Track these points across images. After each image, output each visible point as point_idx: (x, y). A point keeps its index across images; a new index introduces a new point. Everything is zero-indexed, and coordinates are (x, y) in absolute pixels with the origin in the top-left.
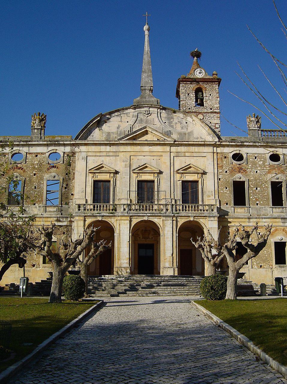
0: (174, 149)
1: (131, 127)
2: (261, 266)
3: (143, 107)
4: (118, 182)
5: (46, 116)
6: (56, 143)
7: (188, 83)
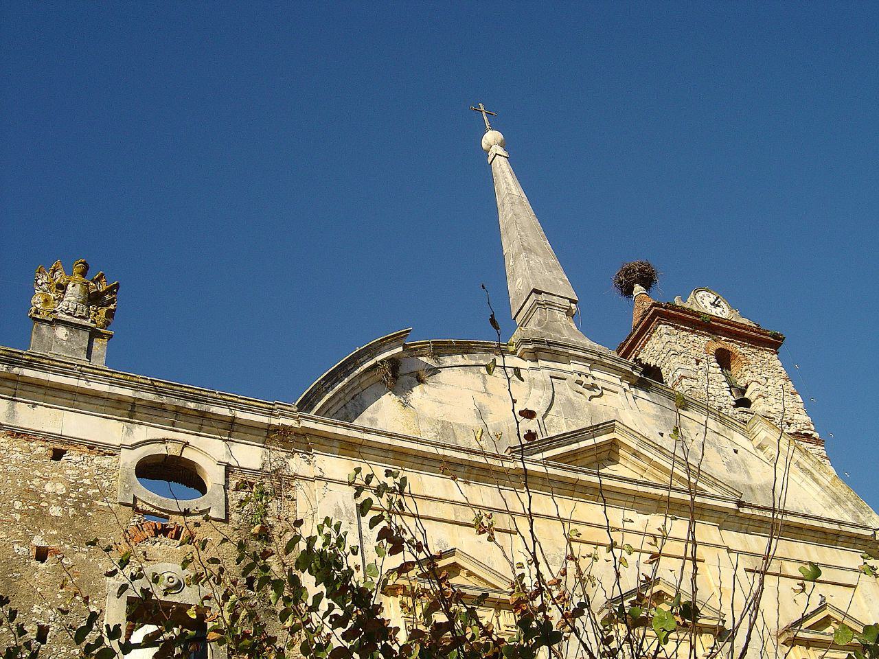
3: (569, 358)
5: (117, 286)
6: (192, 405)
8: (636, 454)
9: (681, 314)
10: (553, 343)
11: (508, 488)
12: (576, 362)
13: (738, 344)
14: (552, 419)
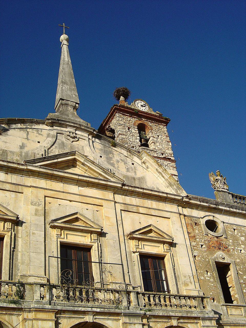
1: (45, 150)
3: (66, 126)
4: (20, 242)
8: (83, 164)
9: (126, 109)
10: (60, 120)
11: (24, 176)
12: (70, 127)
13: (150, 122)
14: (53, 150)
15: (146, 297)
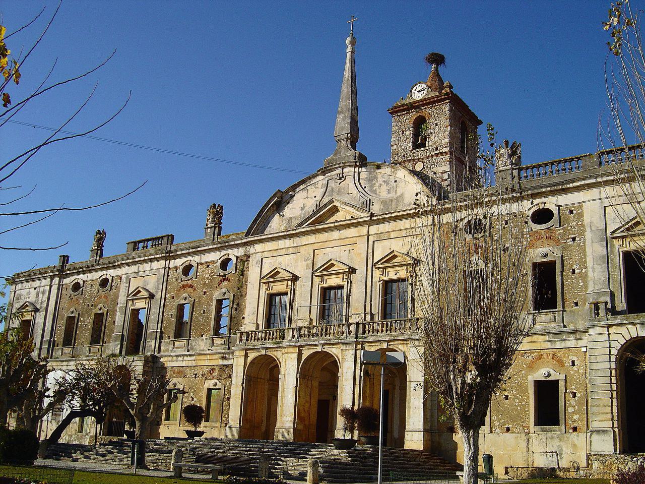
0: (374, 229)
1: (317, 204)
2: (508, 429)
4: (297, 293)
7: (404, 113)
15: (237, 353)
